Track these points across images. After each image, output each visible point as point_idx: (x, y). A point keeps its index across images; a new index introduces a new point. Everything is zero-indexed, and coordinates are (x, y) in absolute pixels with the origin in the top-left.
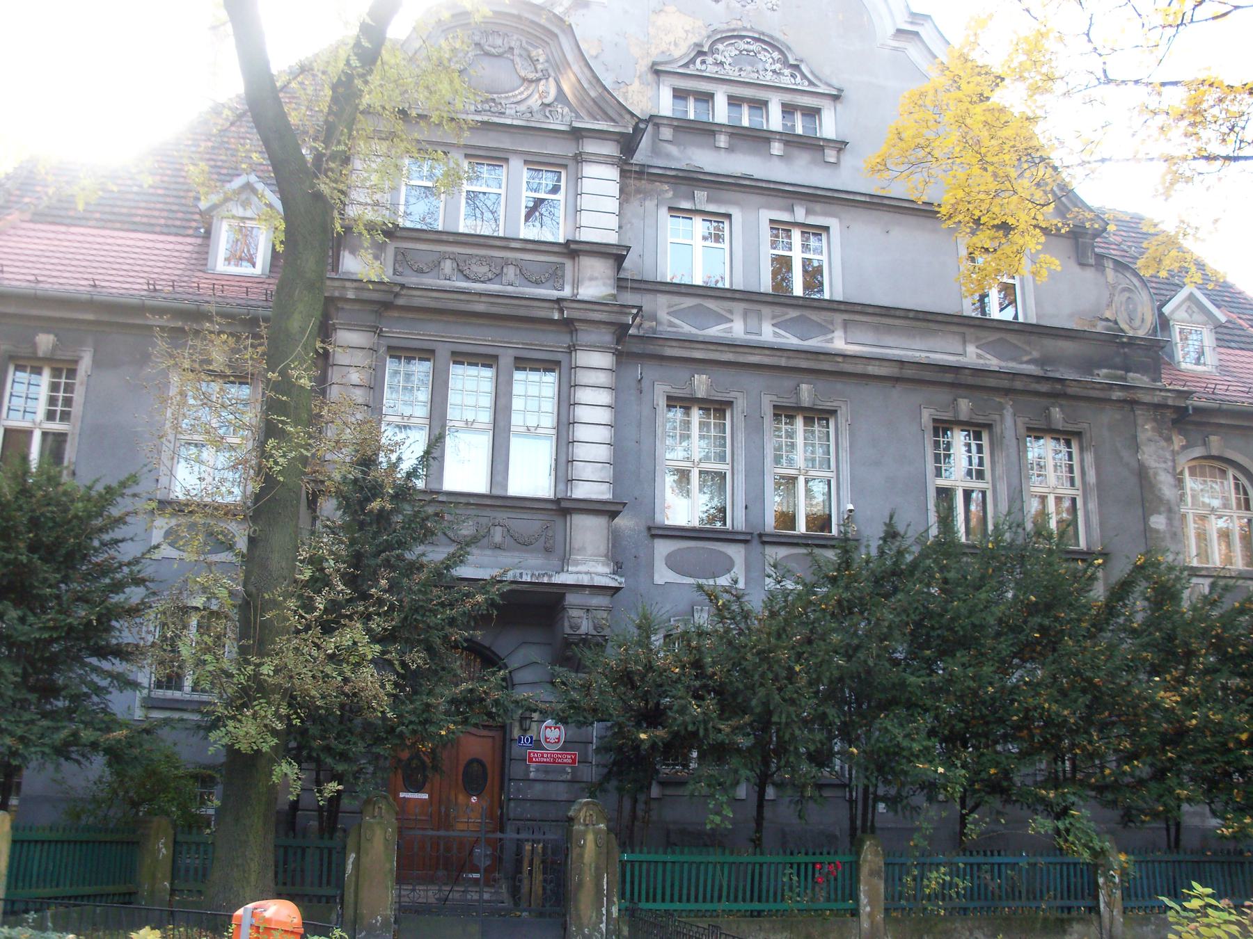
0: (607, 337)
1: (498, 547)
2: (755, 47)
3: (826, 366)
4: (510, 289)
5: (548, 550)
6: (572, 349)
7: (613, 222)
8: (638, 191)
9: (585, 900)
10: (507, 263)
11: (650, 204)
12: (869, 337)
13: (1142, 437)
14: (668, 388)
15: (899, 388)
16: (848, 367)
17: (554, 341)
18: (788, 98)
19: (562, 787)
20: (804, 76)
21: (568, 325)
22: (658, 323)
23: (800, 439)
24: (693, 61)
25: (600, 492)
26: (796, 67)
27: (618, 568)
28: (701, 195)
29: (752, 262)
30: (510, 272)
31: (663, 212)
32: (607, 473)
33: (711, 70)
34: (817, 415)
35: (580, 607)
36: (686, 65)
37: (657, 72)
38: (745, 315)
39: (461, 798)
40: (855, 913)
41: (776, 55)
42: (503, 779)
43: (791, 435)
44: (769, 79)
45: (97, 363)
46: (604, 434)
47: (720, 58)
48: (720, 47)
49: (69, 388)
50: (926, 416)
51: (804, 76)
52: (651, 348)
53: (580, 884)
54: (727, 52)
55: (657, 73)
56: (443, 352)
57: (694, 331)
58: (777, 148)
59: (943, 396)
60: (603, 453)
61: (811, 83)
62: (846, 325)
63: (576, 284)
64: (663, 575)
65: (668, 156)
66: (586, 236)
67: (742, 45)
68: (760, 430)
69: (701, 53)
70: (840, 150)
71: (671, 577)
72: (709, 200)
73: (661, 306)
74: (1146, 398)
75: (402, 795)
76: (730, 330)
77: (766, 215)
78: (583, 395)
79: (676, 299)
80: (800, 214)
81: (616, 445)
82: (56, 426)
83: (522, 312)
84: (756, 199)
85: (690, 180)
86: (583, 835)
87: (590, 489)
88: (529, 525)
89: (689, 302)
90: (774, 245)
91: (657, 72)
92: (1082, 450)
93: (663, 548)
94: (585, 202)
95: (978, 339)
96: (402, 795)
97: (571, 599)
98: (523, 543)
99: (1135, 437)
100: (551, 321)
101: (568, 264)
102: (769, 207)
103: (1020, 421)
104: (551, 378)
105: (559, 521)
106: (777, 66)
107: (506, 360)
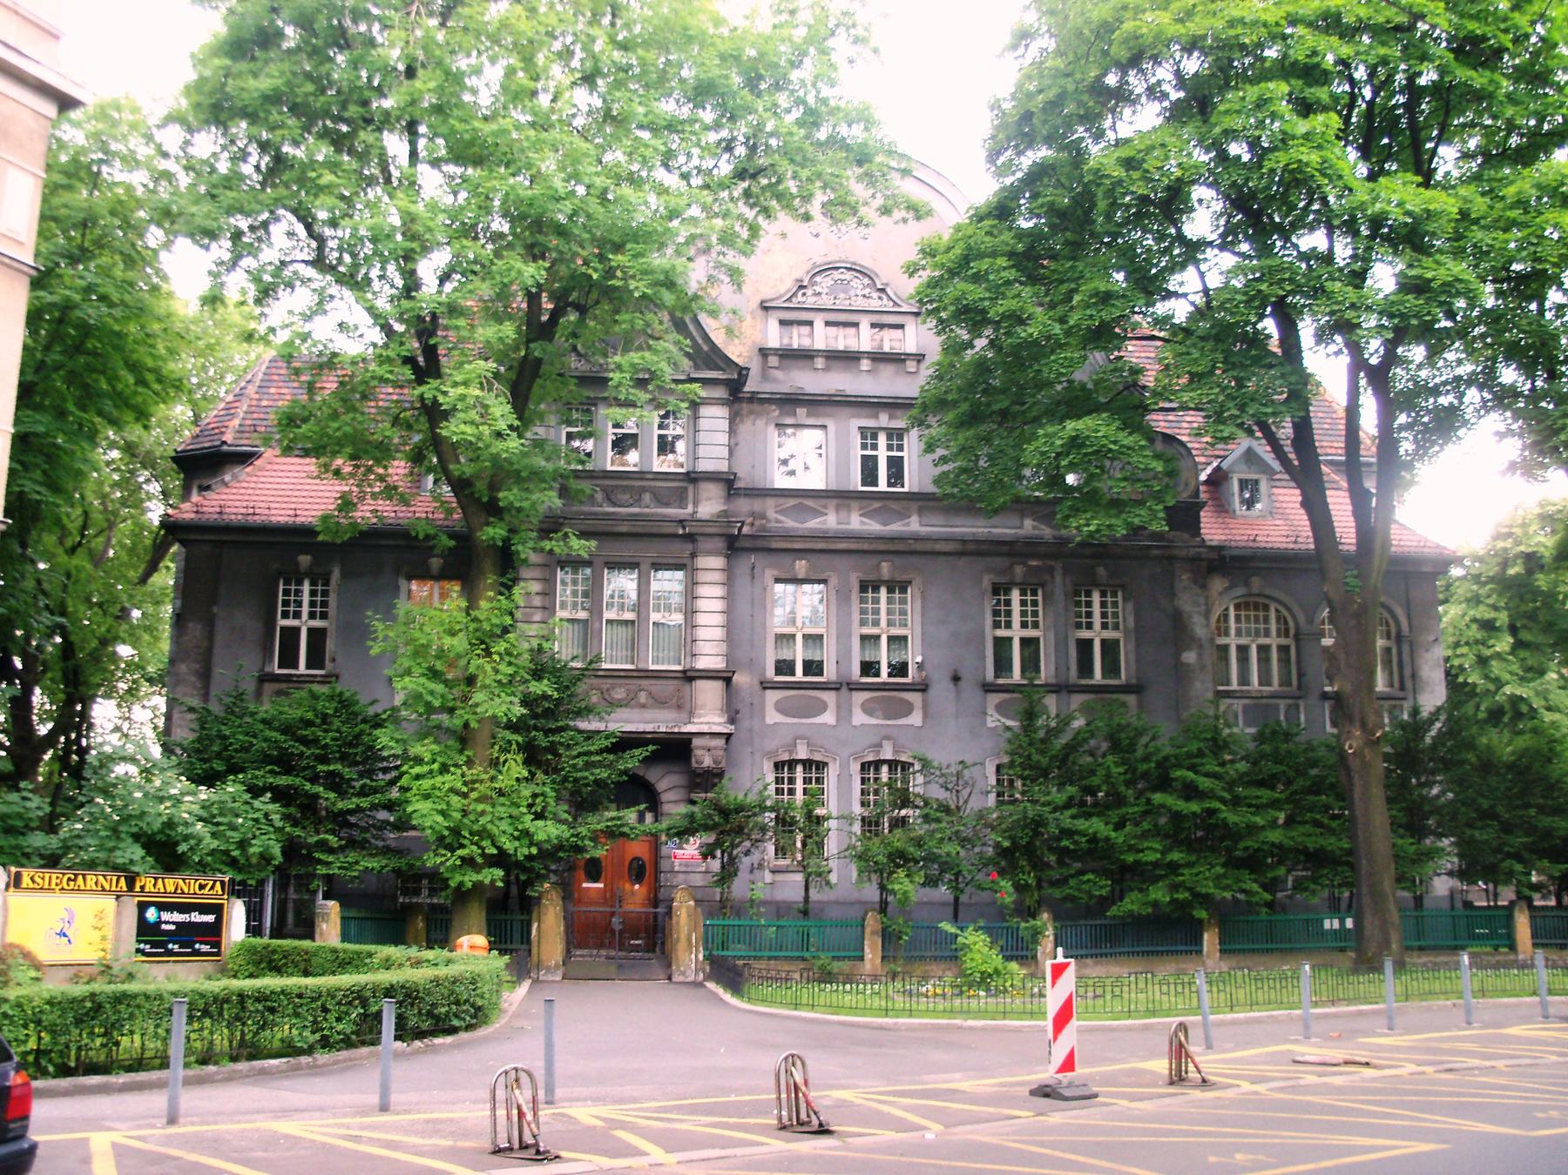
0: (720, 544)
1: (643, 706)
2: (848, 276)
3: (901, 547)
4: (646, 510)
5: (679, 707)
6: (693, 555)
7: (725, 452)
8: (751, 413)
9: (681, 947)
10: (643, 490)
11: (760, 423)
12: (938, 519)
13: (1179, 586)
14: (776, 573)
15: (964, 559)
16: (919, 546)
17: (682, 550)
18: (876, 318)
19: (699, 876)
20: (890, 298)
21: (691, 538)
22: (769, 521)
23: (883, 605)
24: (795, 294)
25: (717, 663)
26: (882, 290)
27: (732, 721)
28: (802, 412)
29: (843, 465)
30: (647, 497)
31: (771, 428)
32: (723, 648)
33: (810, 301)
34: (897, 586)
35: (703, 748)
36: (789, 299)
37: (765, 308)
38: (838, 508)
39: (627, 886)
40: (862, 959)
41: (866, 281)
42: (657, 871)
43: (876, 601)
44: (860, 303)
45: (344, 575)
46: (719, 619)
47: (818, 289)
48: (818, 279)
49: (325, 593)
50: (987, 581)
51: (890, 298)
52: (764, 544)
53: (678, 940)
54: (824, 283)
55: (766, 309)
56: (598, 562)
57: (796, 525)
58: (865, 364)
59: (1001, 562)
60: (718, 633)
61: (895, 304)
62: (920, 512)
63: (696, 504)
64: (773, 717)
65: (775, 380)
66: (704, 466)
67: (836, 275)
68: (848, 599)
69: (801, 287)
70: (919, 361)
71: (779, 718)
72: (809, 415)
73: (770, 507)
74: (1183, 553)
75: (585, 885)
76: (824, 522)
77: (856, 423)
78: (702, 590)
79: (782, 500)
80: (884, 420)
81: (729, 627)
82: (317, 623)
83: (654, 530)
84: (848, 411)
85: (791, 401)
86: (679, 908)
87: (710, 658)
88: (669, 687)
89: (792, 502)
90: (864, 447)
91: (765, 308)
92: (1124, 600)
93: (772, 696)
94: (702, 437)
95: (1034, 513)
96: (585, 885)
97: (696, 742)
98: (660, 702)
99: (1172, 586)
100: (675, 536)
101: (691, 488)
102: (858, 416)
103: (1068, 581)
104: (680, 575)
105: (687, 687)
106: (867, 291)
107: (644, 567)
